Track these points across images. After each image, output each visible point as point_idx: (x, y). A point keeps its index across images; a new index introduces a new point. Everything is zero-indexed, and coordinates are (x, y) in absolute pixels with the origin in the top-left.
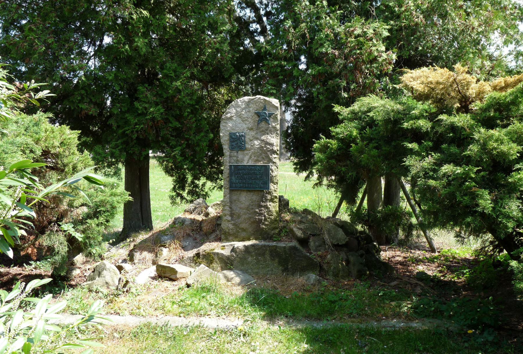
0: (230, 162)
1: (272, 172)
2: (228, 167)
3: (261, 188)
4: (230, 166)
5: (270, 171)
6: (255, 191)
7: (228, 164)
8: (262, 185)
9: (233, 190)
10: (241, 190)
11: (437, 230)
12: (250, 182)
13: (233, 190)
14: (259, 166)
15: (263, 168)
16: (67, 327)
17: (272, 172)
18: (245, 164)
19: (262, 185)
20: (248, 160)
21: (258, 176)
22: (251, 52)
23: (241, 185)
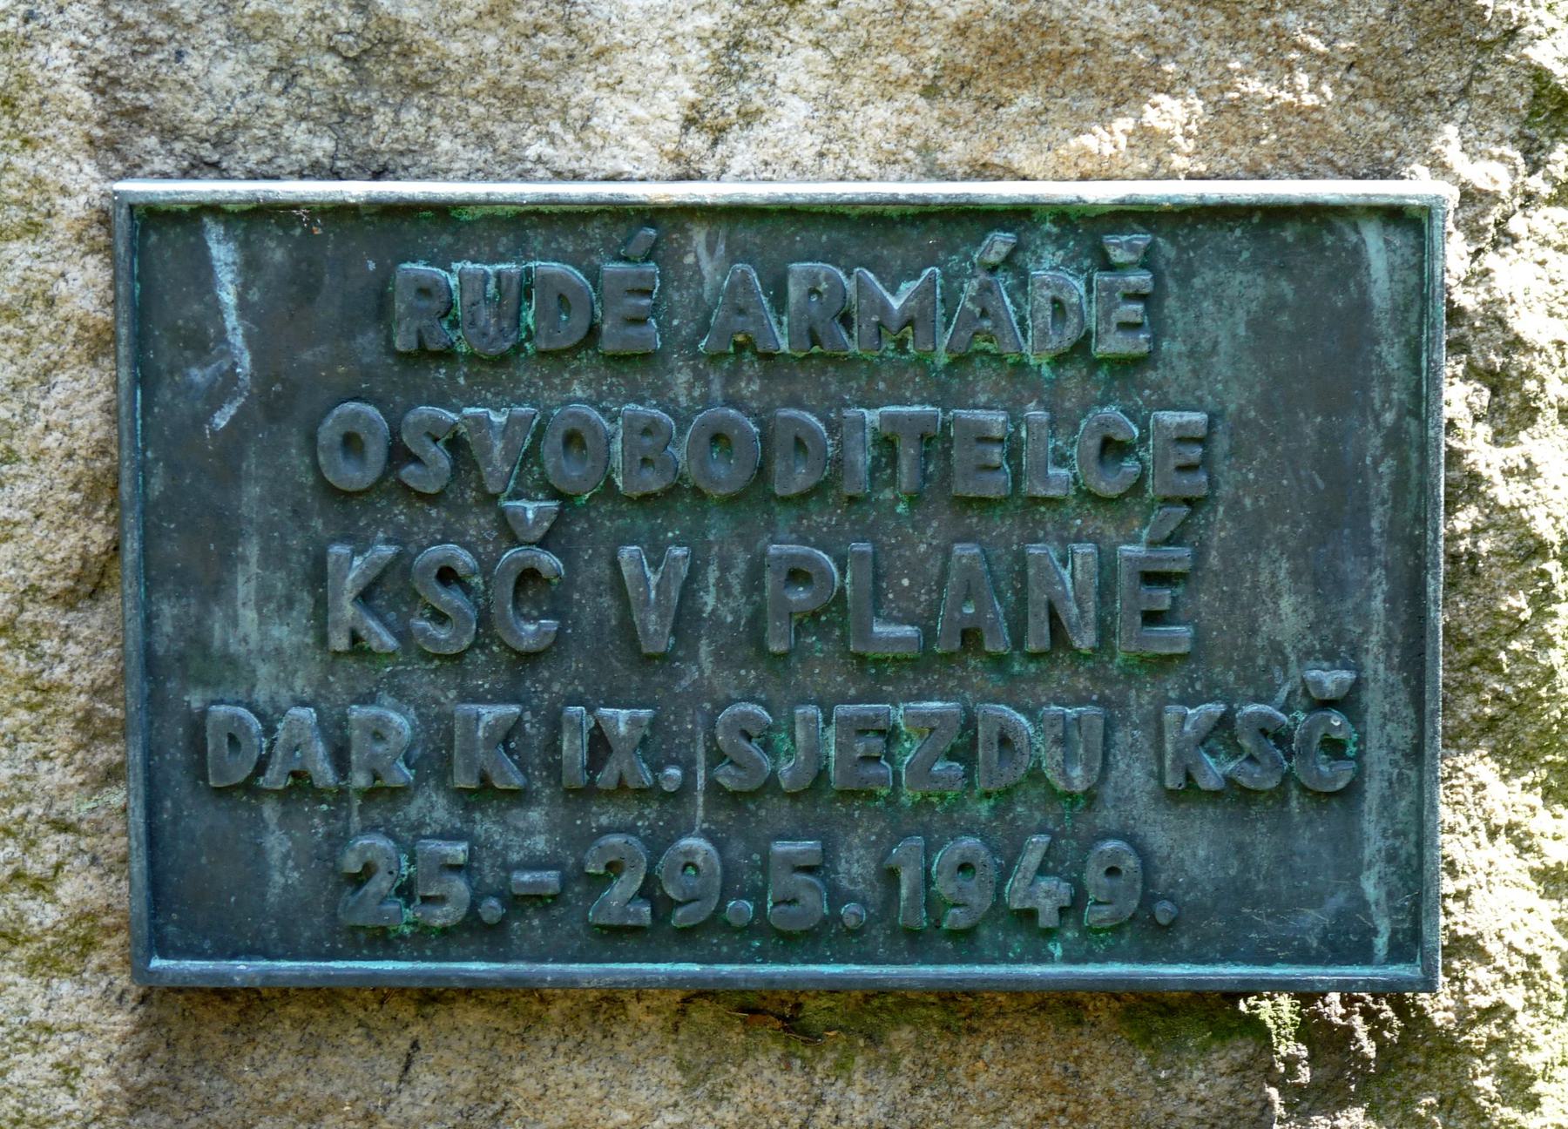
0: (122, 123)
1: (1511, 410)
2: (85, 286)
3: (1150, 932)
4: (151, 242)
5: (1459, 397)
6: (959, 1010)
7: (83, 184)
8: (1193, 850)
9: (249, 1006)
10: (520, 1004)
11: (514, 811)
12: (815, 736)
13: (249, 1006)
14: (1086, 228)
15: (1228, 303)
16: (984, 314)
17: (1511, 410)
18: (626, 148)
19: (1193, 850)
20: (733, 56)
21: (1067, 571)
22: (458, 261)
23: (533, 831)
